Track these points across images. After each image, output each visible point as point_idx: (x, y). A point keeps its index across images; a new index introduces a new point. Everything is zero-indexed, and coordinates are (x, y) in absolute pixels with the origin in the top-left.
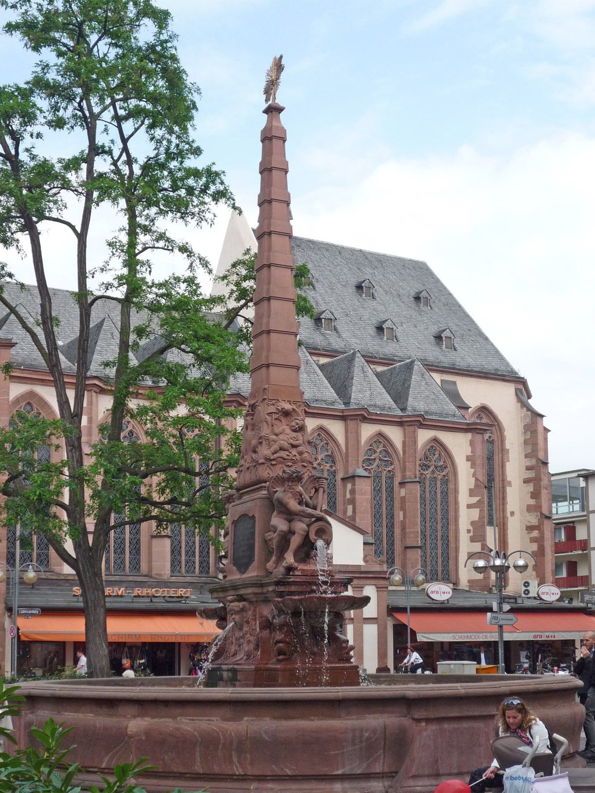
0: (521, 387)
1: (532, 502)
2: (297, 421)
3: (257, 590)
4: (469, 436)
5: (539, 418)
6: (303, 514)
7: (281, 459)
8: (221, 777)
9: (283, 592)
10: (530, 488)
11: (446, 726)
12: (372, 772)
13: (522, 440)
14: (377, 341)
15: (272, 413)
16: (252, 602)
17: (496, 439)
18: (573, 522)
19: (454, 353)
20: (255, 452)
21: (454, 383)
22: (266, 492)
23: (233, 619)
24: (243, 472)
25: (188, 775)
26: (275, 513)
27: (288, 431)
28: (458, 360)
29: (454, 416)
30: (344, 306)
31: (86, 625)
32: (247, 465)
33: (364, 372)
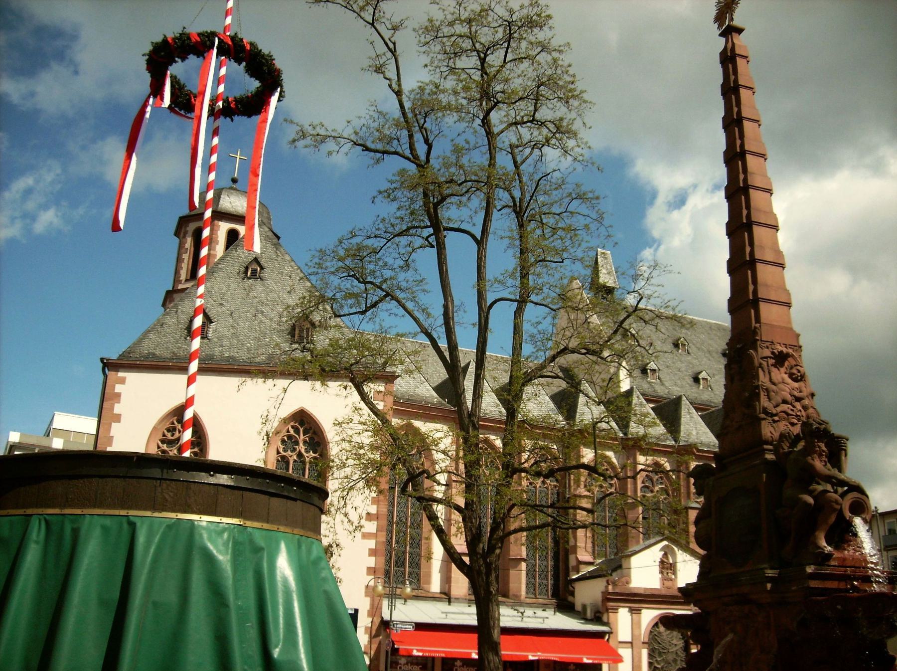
2: (799, 368)
7: (784, 415)
14: (694, 389)
15: (766, 358)
30: (665, 360)
33: (690, 413)
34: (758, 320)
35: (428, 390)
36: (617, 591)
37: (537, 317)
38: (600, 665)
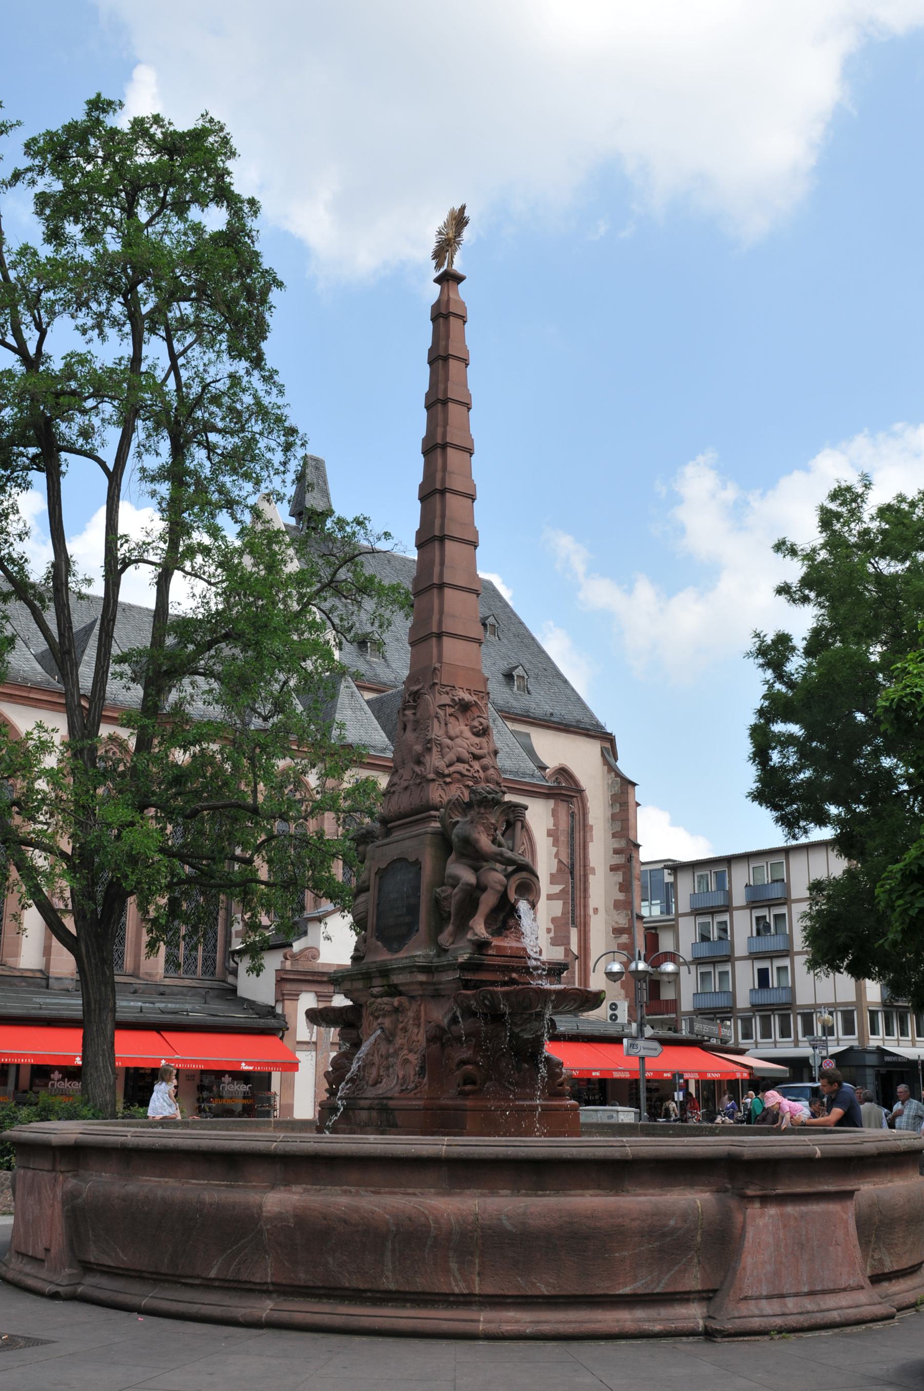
0: (608, 745)
1: (621, 896)
2: (481, 720)
3: (422, 978)
4: (551, 803)
5: (630, 787)
6: (499, 858)
8: (429, 1297)
9: (470, 980)
10: (619, 877)
11: (790, 1209)
12: (678, 1290)
13: (609, 815)
15: (445, 705)
16: (413, 997)
17: (576, 811)
18: (655, 928)
19: (527, 697)
20: (419, 762)
21: (528, 735)
22: (438, 825)
23: (379, 1024)
24: (396, 794)
25: (369, 1294)
26: (453, 856)
27: (467, 733)
28: (533, 706)
29: (533, 776)
31: (84, 1038)
32: (405, 784)
34: (440, 660)
35: (27, 660)
36: (300, 968)
37: (129, 688)
38: (270, 1074)
